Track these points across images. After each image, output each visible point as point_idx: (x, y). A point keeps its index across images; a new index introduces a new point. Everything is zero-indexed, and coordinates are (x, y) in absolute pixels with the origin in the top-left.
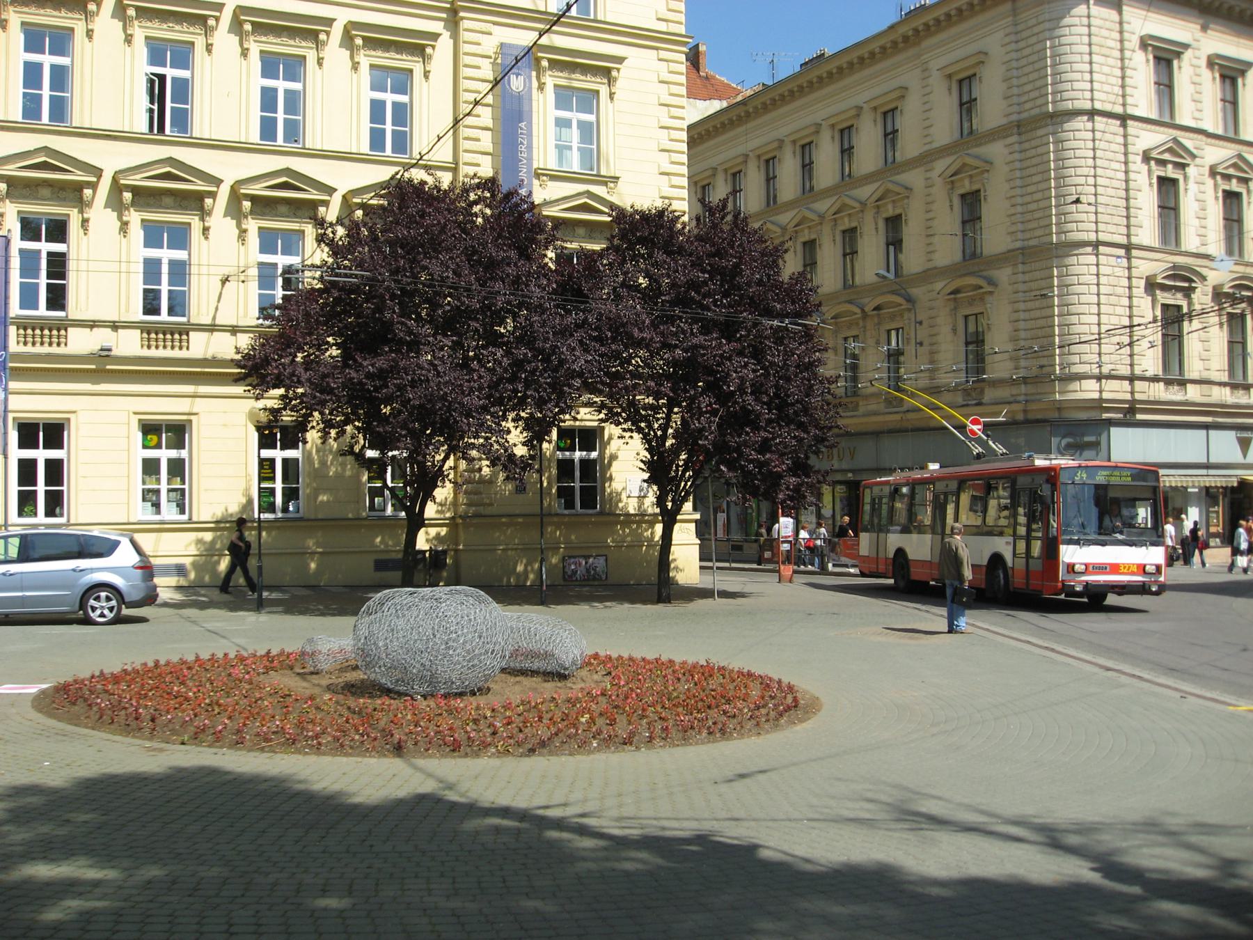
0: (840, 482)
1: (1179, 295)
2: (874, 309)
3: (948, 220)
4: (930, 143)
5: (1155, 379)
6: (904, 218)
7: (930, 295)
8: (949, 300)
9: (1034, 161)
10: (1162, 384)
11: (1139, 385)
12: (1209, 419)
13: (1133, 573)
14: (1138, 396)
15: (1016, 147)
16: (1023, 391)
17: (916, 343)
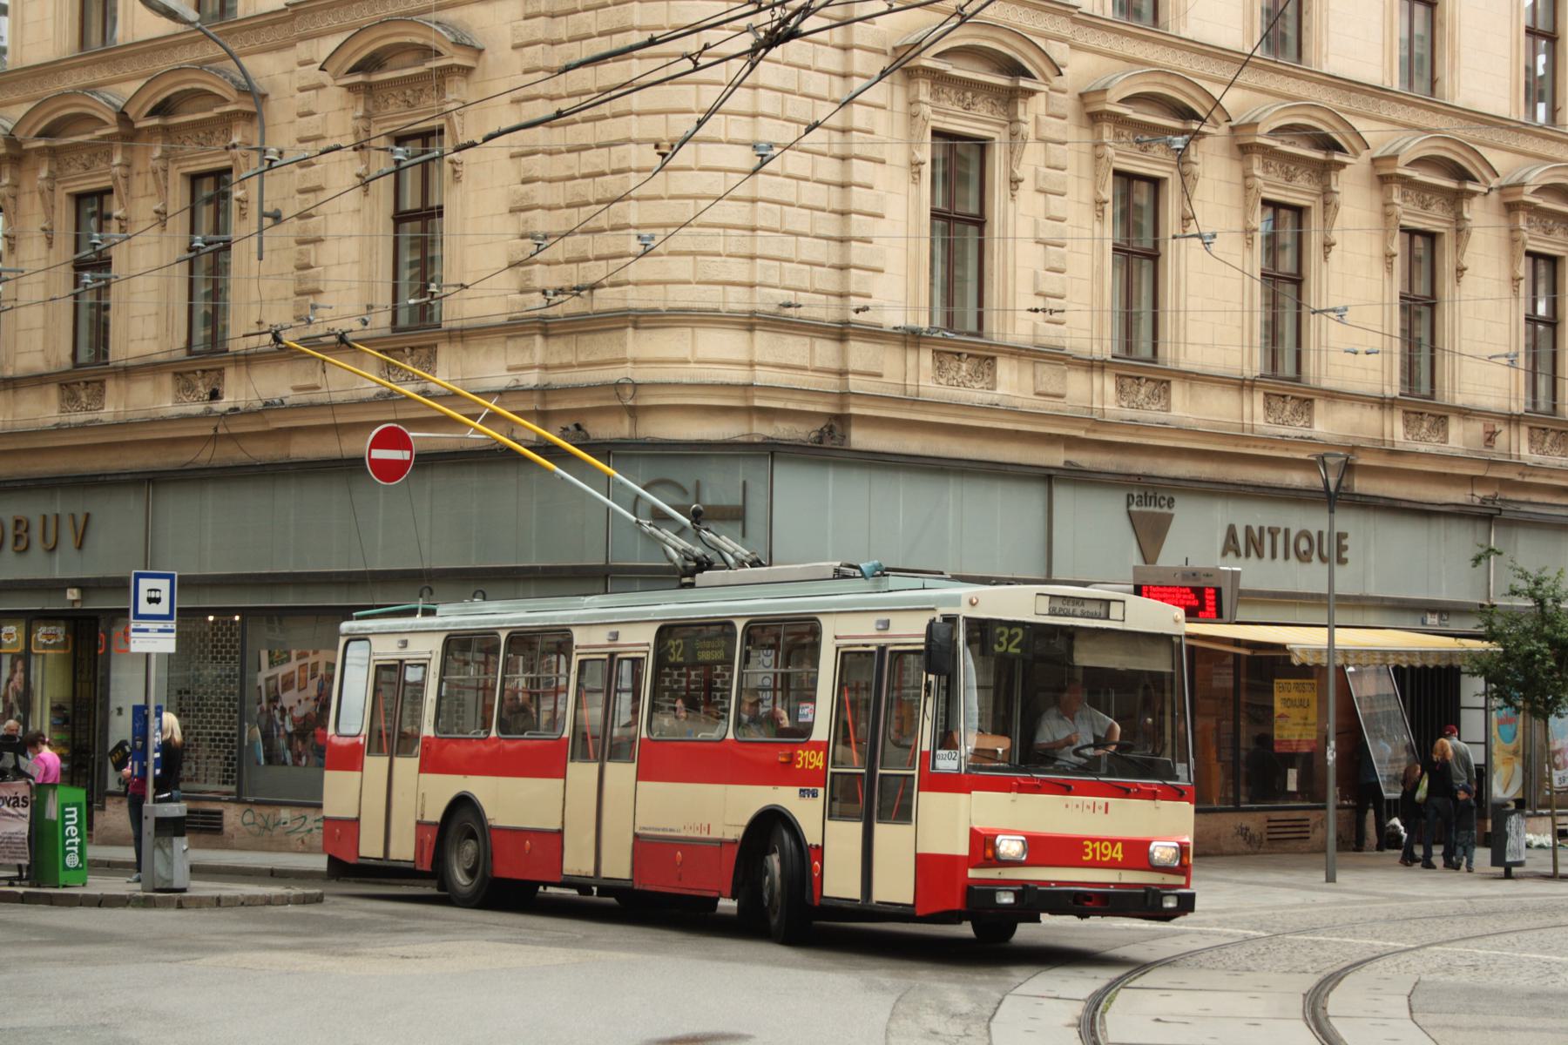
0: (1488, 754)
1: (982, 109)
2: (154, 112)
5: (911, 338)
8: (351, 88)
10: (926, 357)
11: (860, 354)
12: (1056, 457)
13: (1112, 865)
14: (856, 384)
16: (538, 359)
17: (263, 215)
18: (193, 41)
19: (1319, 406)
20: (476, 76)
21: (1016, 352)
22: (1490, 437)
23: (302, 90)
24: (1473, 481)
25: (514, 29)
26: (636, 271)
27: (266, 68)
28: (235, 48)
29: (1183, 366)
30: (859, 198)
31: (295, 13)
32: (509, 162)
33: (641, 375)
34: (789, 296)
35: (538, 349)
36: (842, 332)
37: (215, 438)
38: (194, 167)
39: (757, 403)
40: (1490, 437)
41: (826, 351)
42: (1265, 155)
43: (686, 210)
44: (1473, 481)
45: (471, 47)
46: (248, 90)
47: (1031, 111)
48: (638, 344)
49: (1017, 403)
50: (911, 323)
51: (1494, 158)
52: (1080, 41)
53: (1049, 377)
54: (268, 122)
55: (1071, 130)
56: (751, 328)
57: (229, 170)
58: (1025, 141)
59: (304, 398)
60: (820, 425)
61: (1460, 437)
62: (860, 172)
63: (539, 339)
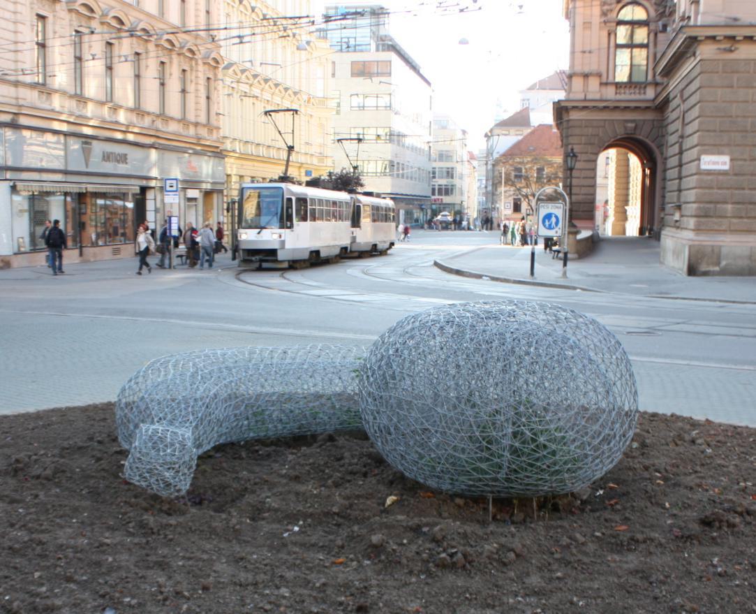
5: (33, 86)
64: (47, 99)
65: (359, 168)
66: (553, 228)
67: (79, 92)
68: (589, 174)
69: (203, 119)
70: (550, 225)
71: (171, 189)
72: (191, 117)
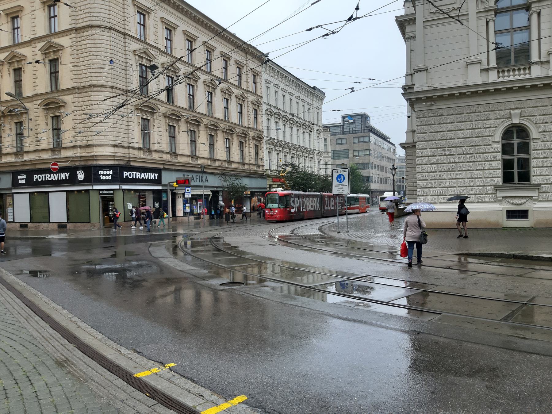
3: (43, 71)
4: (35, 34)
5: (139, 149)
6: (23, 69)
7: (34, 108)
9: (83, 47)
10: (142, 152)
11: (131, 151)
14: (131, 156)
15: (74, 40)
18: (16, 101)
19: (199, 159)
20: (66, 107)
21: (155, 151)
22: (222, 163)
23: (35, 109)
24: (220, 169)
25: (72, 100)
26: (95, 138)
27: (28, 105)
28: (23, 102)
29: (180, 153)
30: (130, 128)
31: (33, 97)
32: (72, 121)
33: (96, 154)
34: (120, 142)
35: (79, 150)
36: (129, 148)
37: (23, 165)
38: (16, 121)
39: (116, 158)
40: (222, 163)
41: (126, 151)
42: (141, 110)
43: (103, 129)
44: (220, 169)
45: (65, 103)
46: (25, 108)
47: (156, 116)
48: (95, 149)
49: (156, 159)
50: (139, 146)
51: (221, 125)
52: (163, 105)
53: (160, 155)
54: (29, 114)
55: (161, 118)
56: (114, 147)
57: (60, 116)
58: (155, 120)
59: (38, 158)
60: (126, 162)
61: (218, 164)
62: (130, 123)
63: (79, 149)
64: (150, 154)
65: (31, 121)
66: (342, 182)
67: (229, 159)
68: (348, 154)
69: (253, 161)
70: (341, 180)
71: (188, 192)
72: (247, 161)
